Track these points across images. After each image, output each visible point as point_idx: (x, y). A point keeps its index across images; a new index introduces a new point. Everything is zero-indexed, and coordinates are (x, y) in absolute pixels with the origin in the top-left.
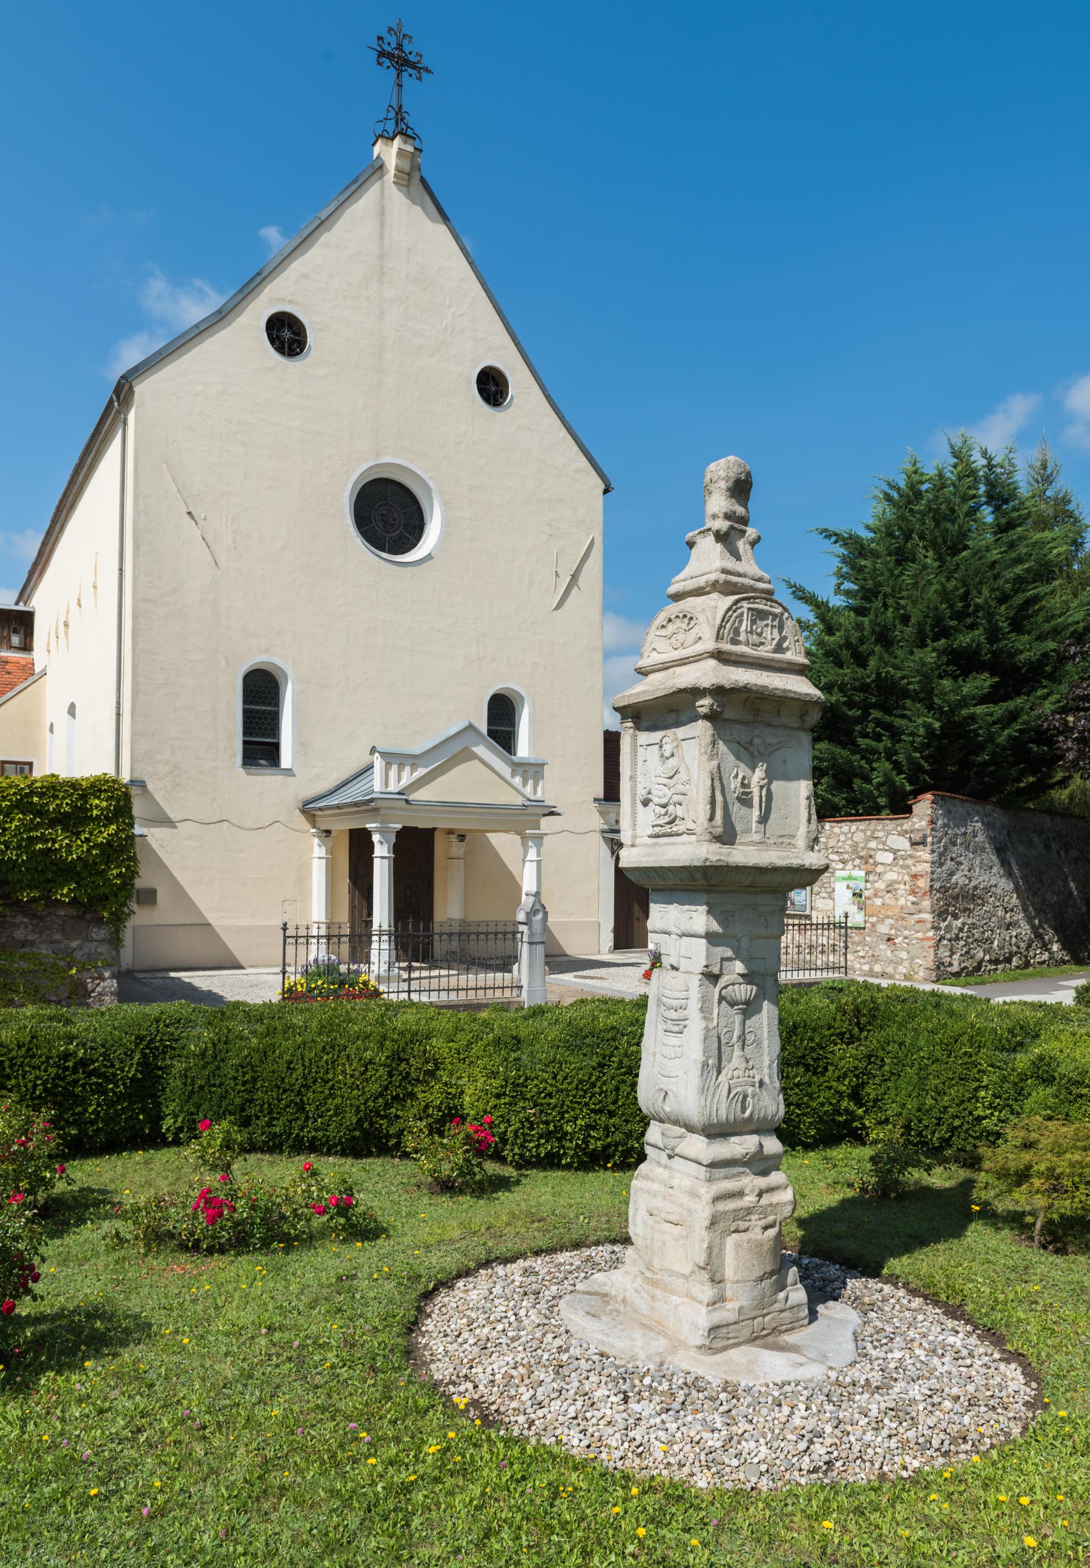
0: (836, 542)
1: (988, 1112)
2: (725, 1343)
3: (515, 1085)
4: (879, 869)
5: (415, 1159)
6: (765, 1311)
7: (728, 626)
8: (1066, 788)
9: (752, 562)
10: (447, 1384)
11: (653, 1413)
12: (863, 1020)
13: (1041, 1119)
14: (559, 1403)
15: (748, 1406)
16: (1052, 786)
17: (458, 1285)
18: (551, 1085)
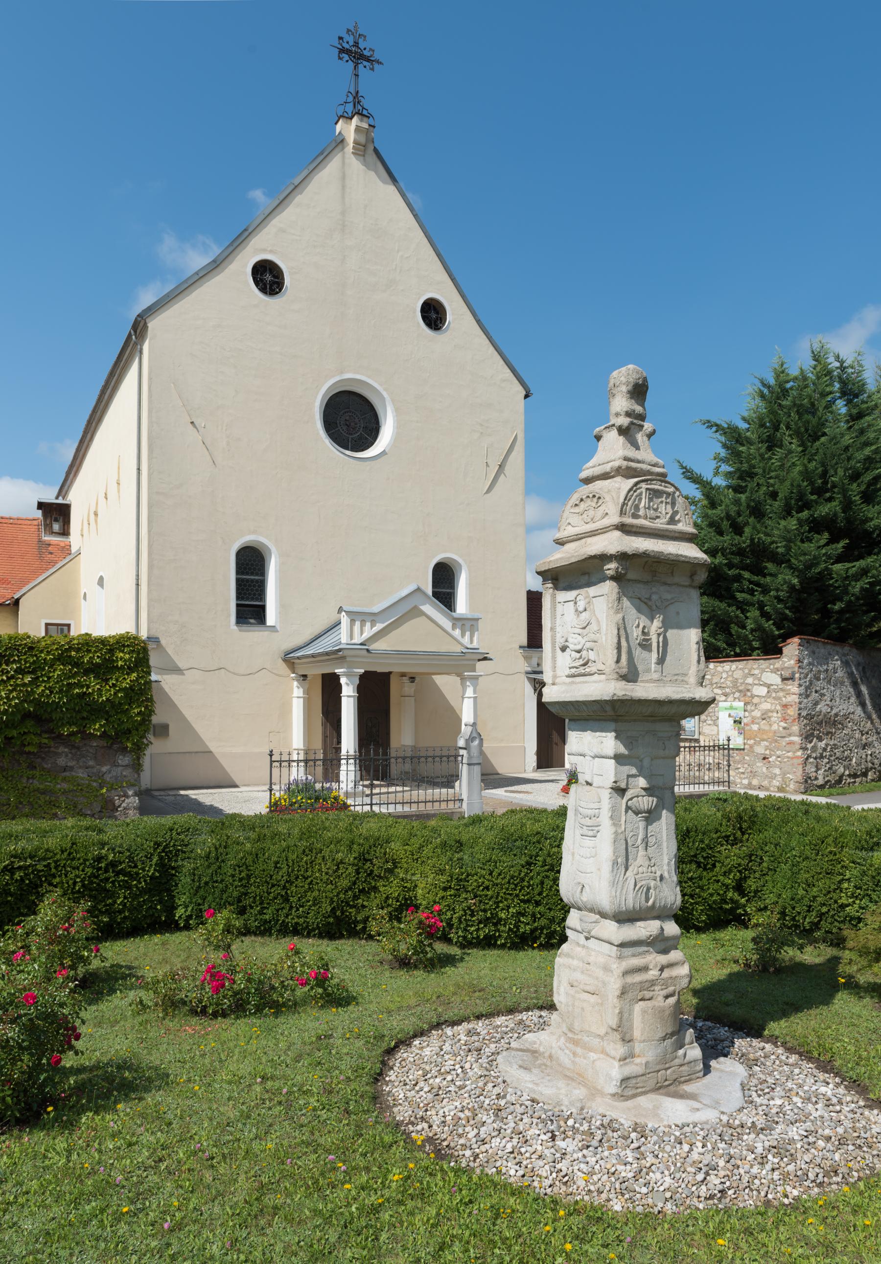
0: (716, 432)
4: (756, 700)
6: (667, 1065)
7: (630, 503)
9: (649, 451)
10: (407, 1124)
11: (576, 1149)
12: (745, 825)
14: (498, 1140)
15: (655, 1144)
17: (415, 1043)
18: (488, 880)
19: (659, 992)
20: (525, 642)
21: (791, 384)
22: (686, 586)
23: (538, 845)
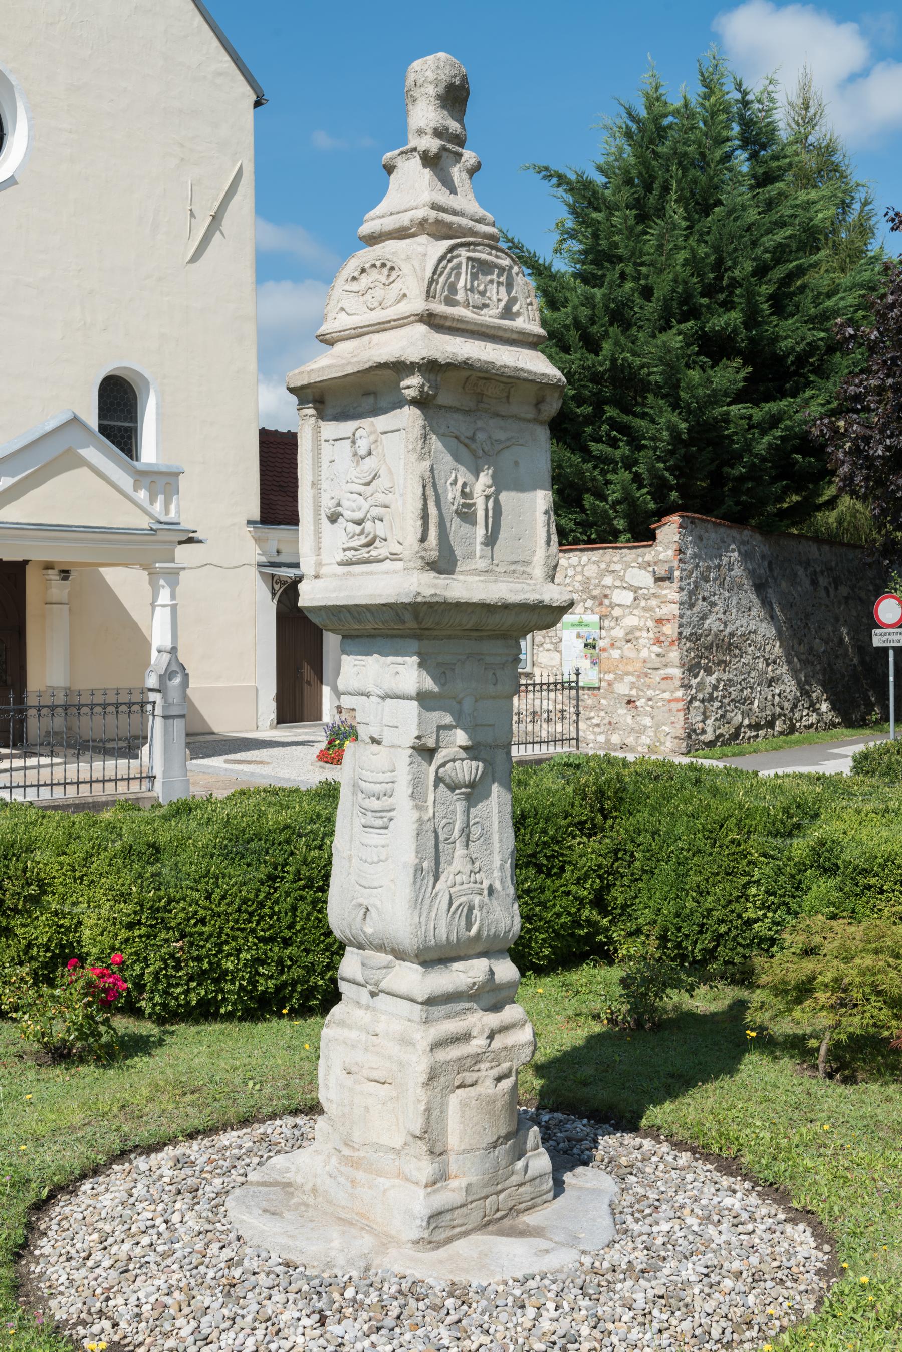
0: (559, 185)
1: (760, 913)
2: (449, 1233)
3: (154, 910)
4: (617, 612)
5: (14, 1020)
6: (500, 1187)
7: (442, 280)
8: (833, 509)
9: (471, 196)
10: (74, 1326)
11: (360, 1334)
12: (608, 804)
13: (823, 919)
14: (232, 1334)
15: (483, 1313)
16: (819, 508)
17: (83, 1188)
18: (205, 908)
19: (487, 1072)
20: (256, 515)
21: (670, 119)
22: (529, 421)
23: (286, 847)
